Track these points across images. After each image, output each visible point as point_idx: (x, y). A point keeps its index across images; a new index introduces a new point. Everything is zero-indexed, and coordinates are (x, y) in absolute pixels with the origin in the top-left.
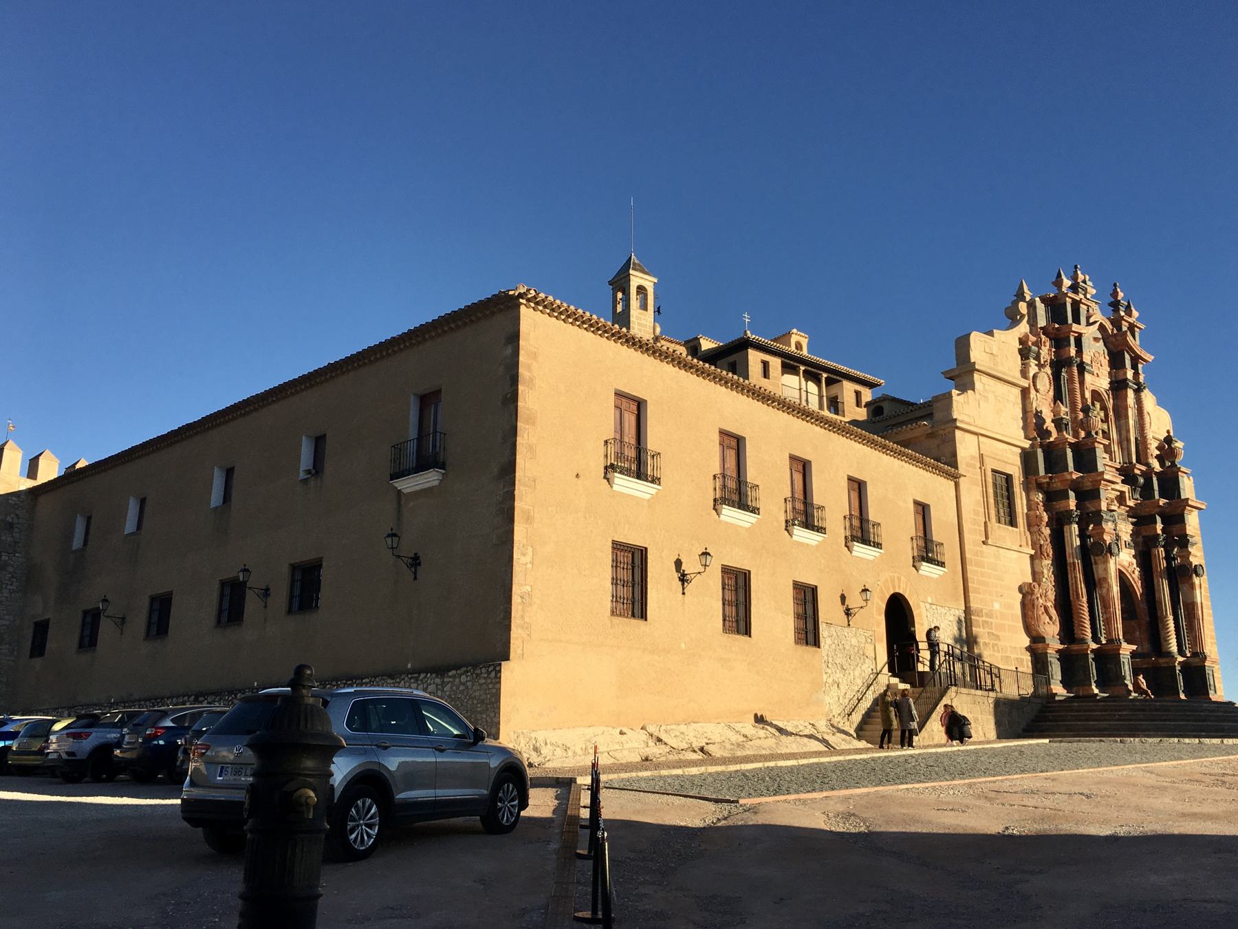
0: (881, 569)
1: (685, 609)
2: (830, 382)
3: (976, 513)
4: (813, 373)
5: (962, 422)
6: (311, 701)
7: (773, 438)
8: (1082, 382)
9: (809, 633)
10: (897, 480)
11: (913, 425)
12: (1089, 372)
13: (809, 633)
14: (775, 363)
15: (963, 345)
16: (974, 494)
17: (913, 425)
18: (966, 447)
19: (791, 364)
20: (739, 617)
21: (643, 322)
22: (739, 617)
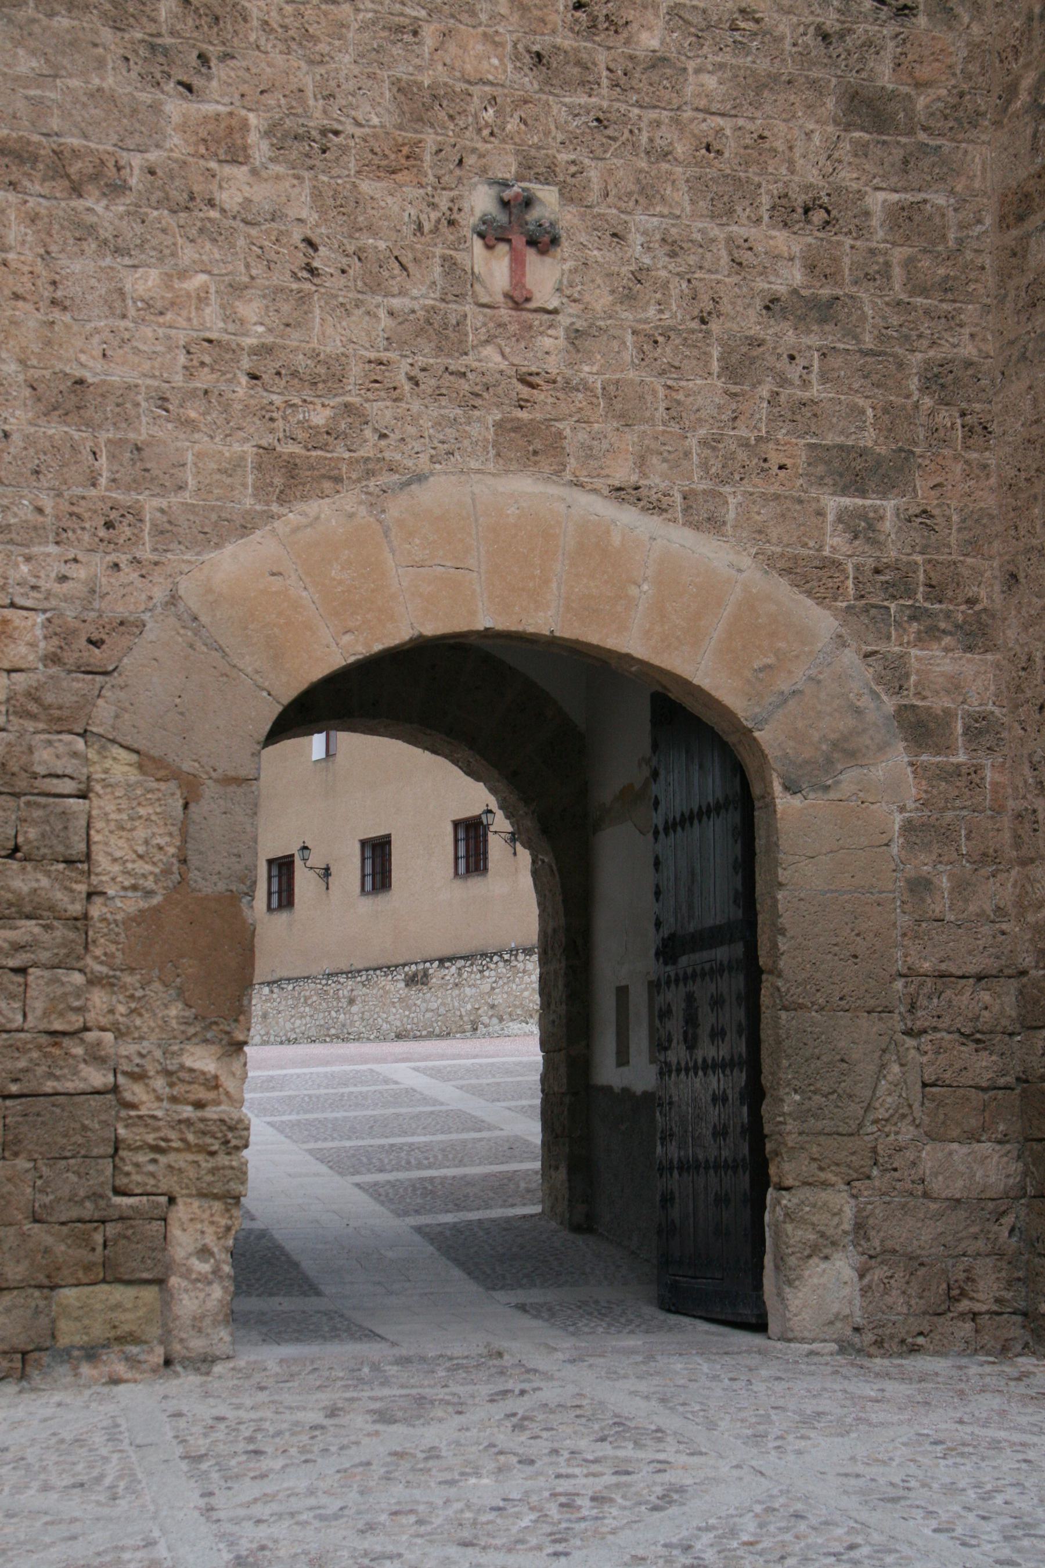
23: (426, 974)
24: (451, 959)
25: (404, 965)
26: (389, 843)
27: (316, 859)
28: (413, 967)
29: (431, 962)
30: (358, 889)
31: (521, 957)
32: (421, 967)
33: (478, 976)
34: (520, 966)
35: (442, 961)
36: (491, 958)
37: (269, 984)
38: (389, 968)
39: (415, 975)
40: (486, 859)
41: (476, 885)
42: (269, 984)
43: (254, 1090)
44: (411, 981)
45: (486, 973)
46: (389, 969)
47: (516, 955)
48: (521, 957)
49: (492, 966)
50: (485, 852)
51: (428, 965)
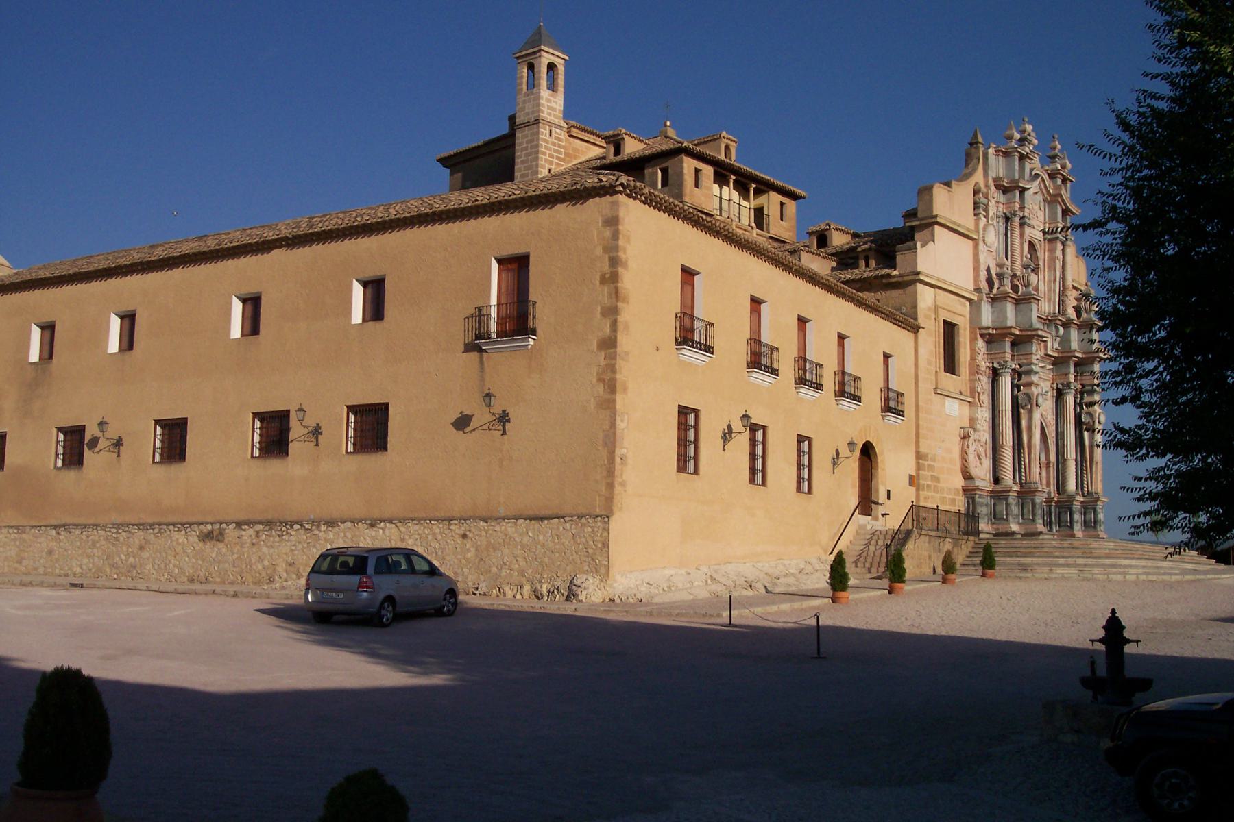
0: (838, 424)
1: (724, 462)
2: (758, 192)
3: (929, 363)
4: (745, 183)
5: (925, 275)
6: (1149, 366)
7: (731, 278)
8: (1022, 235)
9: (804, 483)
10: (869, 335)
11: (875, 265)
12: (1029, 226)
13: (804, 483)
14: (708, 171)
15: (925, 192)
16: (930, 342)
17: (875, 265)
18: (925, 297)
19: (722, 173)
20: (757, 473)
21: (553, 105)
22: (757, 473)
23: (221, 533)
24: (250, 523)
25: (199, 524)
26: (186, 424)
27: (112, 433)
28: (209, 527)
29: (228, 524)
30: (814, 443)
31: (323, 528)
32: (217, 526)
33: (277, 539)
34: (321, 535)
35: (239, 524)
36: (292, 526)
37: (55, 527)
38: (183, 525)
39: (211, 533)
40: (678, 455)
41: (275, 466)
42: (55, 527)
43: (1005, 318)
44: (208, 537)
45: (286, 537)
46: (184, 526)
47: (319, 525)
48: (323, 528)
49: (293, 533)
50: (678, 460)
51: (224, 526)
